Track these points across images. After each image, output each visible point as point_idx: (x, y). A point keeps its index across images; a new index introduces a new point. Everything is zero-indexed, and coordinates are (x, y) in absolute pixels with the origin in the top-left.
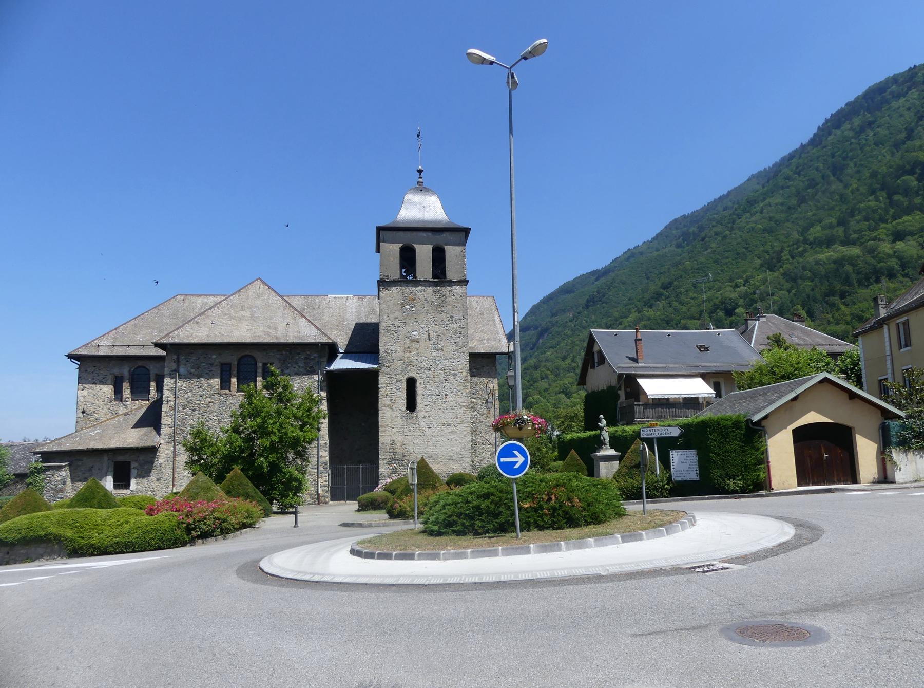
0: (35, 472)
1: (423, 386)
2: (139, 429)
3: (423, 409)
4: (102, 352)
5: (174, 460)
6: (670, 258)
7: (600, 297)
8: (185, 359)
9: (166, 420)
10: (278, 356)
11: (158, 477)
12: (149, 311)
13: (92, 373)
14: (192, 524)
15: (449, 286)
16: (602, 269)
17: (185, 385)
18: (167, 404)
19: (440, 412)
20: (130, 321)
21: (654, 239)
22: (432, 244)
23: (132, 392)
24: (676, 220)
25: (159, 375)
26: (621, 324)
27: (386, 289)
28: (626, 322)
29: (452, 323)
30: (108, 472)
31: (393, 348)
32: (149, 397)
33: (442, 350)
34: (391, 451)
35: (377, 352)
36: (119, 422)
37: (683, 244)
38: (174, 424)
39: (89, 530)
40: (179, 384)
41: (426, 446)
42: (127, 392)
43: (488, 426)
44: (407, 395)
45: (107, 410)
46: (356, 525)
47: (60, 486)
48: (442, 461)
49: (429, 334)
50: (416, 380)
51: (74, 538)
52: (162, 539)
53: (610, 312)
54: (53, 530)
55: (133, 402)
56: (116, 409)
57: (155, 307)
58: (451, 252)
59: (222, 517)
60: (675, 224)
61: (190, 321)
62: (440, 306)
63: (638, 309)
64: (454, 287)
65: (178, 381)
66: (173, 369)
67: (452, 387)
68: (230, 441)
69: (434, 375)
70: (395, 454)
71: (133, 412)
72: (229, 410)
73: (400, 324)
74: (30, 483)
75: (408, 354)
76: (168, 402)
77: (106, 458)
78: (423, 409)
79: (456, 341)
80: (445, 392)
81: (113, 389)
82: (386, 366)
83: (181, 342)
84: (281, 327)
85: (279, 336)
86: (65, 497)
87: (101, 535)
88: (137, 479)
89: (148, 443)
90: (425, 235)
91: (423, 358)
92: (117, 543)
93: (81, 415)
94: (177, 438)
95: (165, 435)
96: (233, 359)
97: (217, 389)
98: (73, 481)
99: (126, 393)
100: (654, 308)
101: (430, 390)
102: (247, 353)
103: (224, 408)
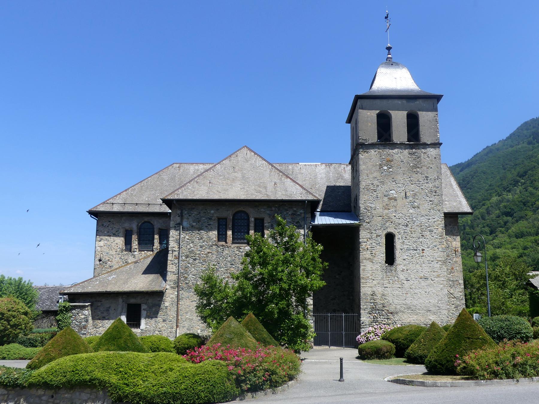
0: (64, 310)
1: (401, 241)
2: (148, 275)
3: (401, 263)
4: (116, 208)
5: (178, 304)
6: (523, 153)
7: (465, 184)
8: (188, 213)
9: (171, 268)
10: (268, 212)
11: (164, 318)
12: (151, 176)
13: (108, 226)
14: (242, 376)
15: (423, 149)
16: (465, 162)
17: (187, 237)
18: (172, 253)
19: (418, 266)
20: (137, 184)
21: (508, 138)
22: (406, 111)
23: (139, 244)
24: (526, 123)
25: (161, 229)
26: (484, 205)
27: (365, 152)
28: (489, 203)
29: (427, 183)
30: (122, 312)
31: (373, 206)
32: (153, 249)
33: (419, 208)
34: (371, 301)
35: (357, 207)
36: (131, 269)
37: (533, 142)
38: (178, 272)
39: (133, 376)
40: (182, 236)
41: (405, 298)
42: (135, 244)
43: (452, 281)
44: (386, 249)
45: (119, 259)
46: (416, 383)
47: (83, 323)
48: (420, 312)
49: (406, 193)
50: (395, 235)
51: (119, 384)
52: (212, 391)
53: (473, 196)
54: (98, 374)
55: (139, 252)
56: (126, 258)
57: (157, 173)
58: (424, 117)
59: (271, 368)
60: (526, 125)
61: (191, 181)
62: (416, 167)
63: (498, 193)
64: (428, 149)
65: (181, 233)
66: (178, 222)
67: (428, 243)
68: (241, 288)
69: (411, 231)
70: (375, 304)
71: (142, 260)
72: (225, 260)
73: (378, 183)
74: (60, 320)
75: (386, 211)
76: (173, 251)
77: (120, 300)
78: (401, 263)
79: (431, 199)
80: (422, 247)
81: (124, 241)
82: (367, 222)
83: (185, 198)
84: (270, 186)
85: (270, 194)
86: (87, 333)
87: (146, 383)
88: (147, 319)
89: (157, 288)
90: (400, 102)
91: (401, 215)
92: (164, 393)
93: (98, 263)
94: (180, 284)
95: (170, 281)
96: (229, 214)
97: (215, 241)
98: (93, 319)
99: (134, 244)
100: (512, 192)
101: (407, 245)
102: (241, 209)
103: (221, 258)
